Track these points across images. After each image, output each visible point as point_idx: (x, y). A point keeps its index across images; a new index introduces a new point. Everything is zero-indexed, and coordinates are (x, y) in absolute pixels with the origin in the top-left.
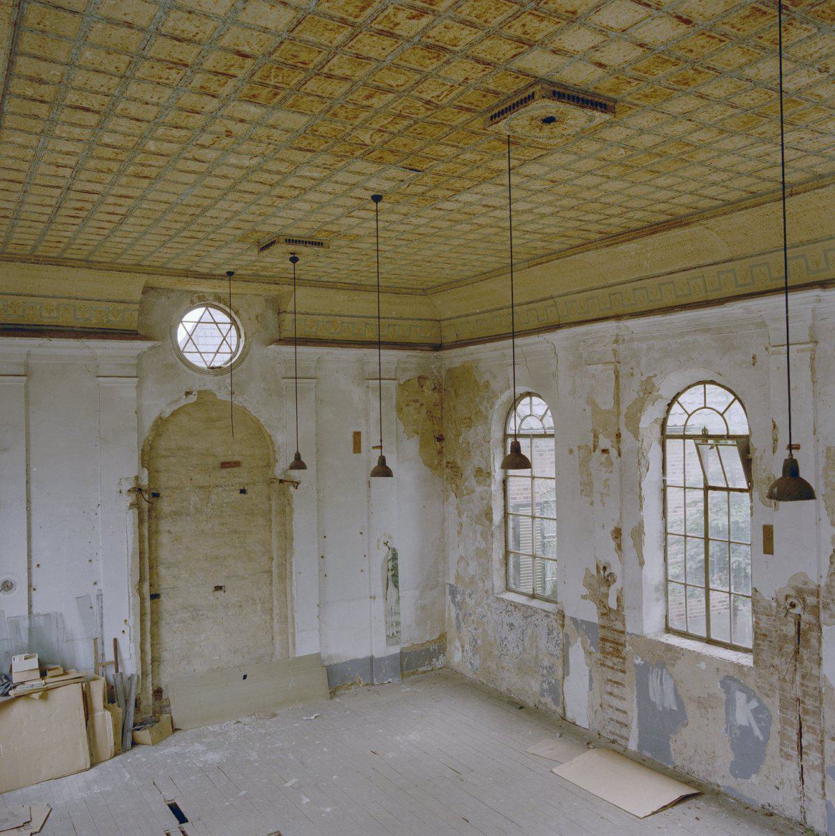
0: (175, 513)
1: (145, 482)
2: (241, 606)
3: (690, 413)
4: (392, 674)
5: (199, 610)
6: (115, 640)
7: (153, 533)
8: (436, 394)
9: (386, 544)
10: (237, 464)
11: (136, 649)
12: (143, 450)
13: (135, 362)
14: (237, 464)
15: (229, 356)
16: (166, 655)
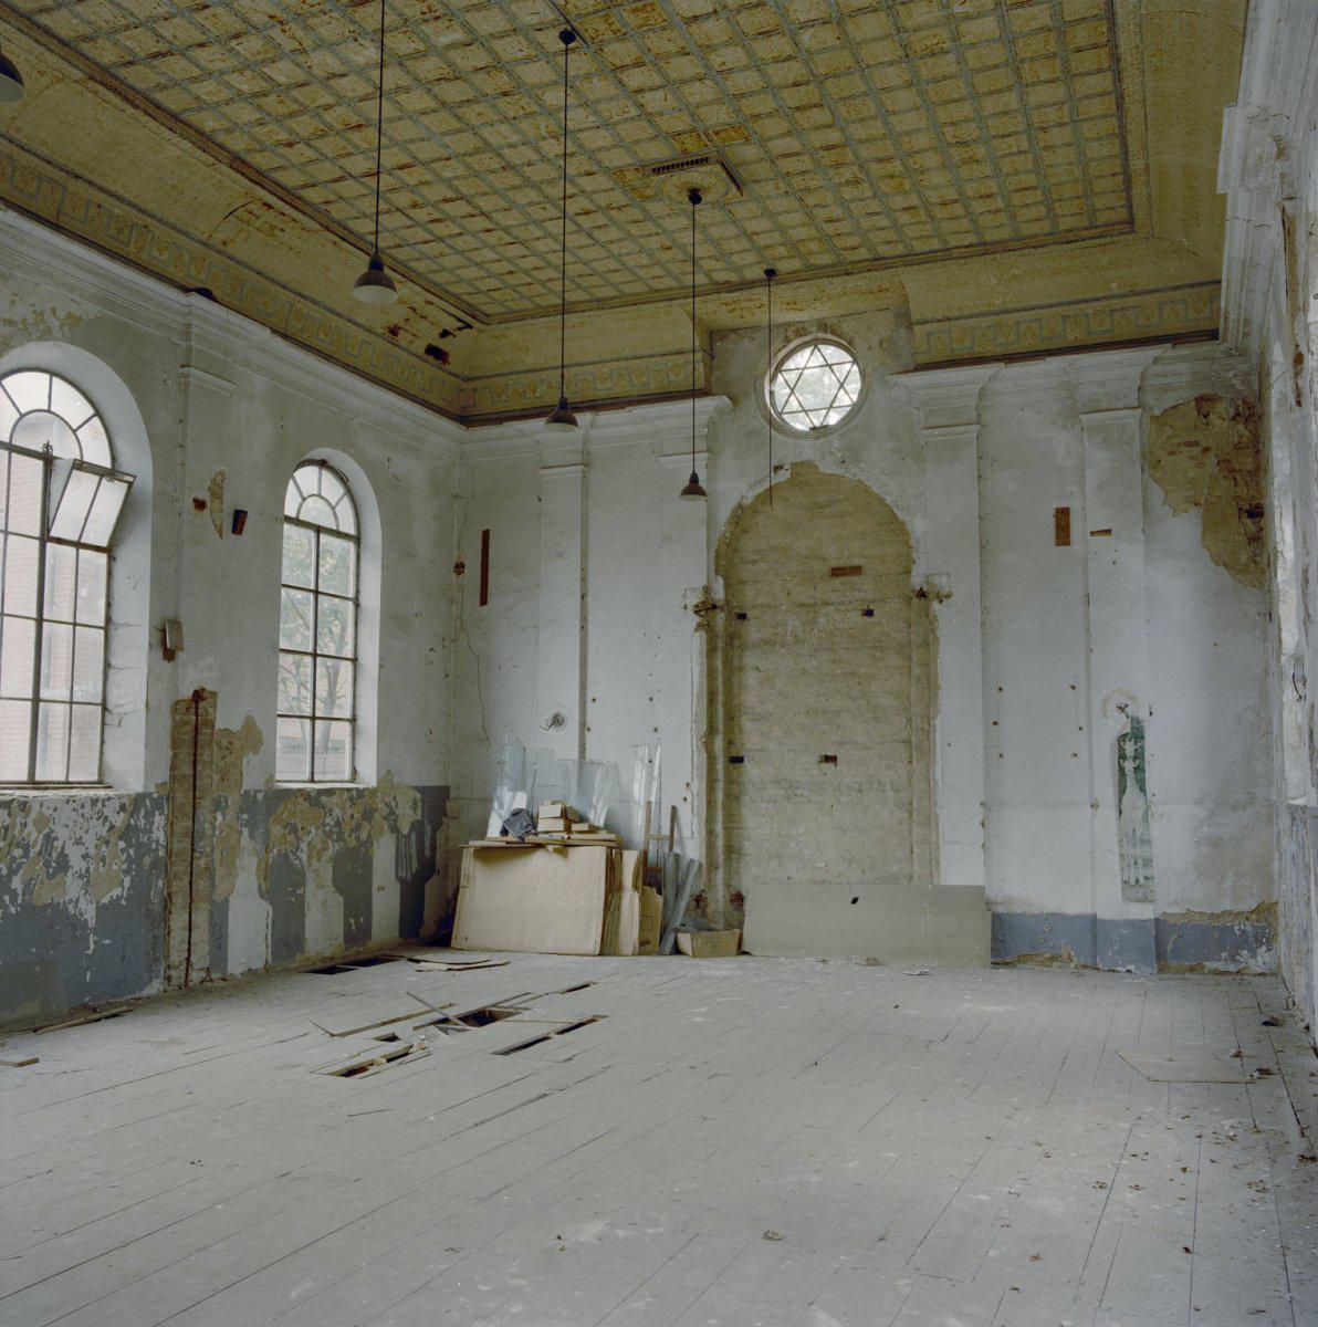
0: (766, 642)
1: (719, 594)
2: (861, 791)
4: (1136, 958)
5: (797, 788)
6: (674, 809)
7: (732, 670)
8: (1241, 427)
9: (1122, 709)
10: (856, 570)
11: (699, 825)
12: (717, 552)
14: (856, 570)
16: (749, 847)
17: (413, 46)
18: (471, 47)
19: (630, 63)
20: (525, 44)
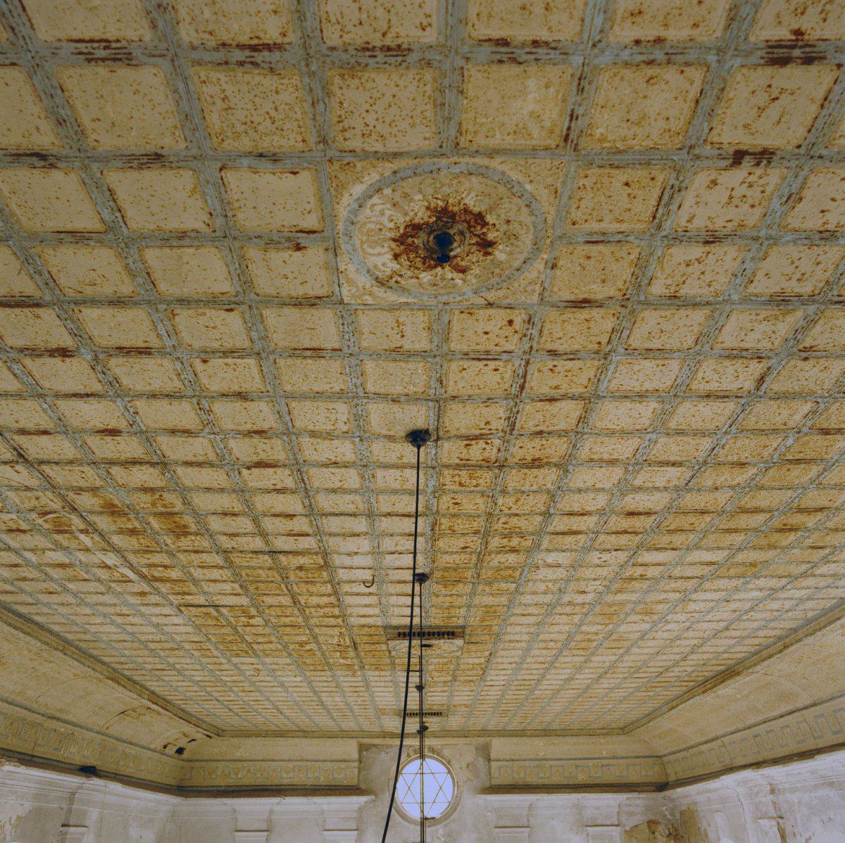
13: (355, 815)
15: (447, 804)
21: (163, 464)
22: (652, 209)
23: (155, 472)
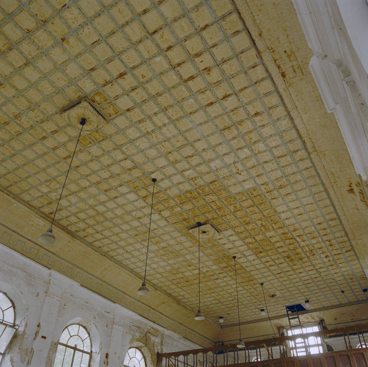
3: (71, 335)
17: (200, 168)
18: (182, 170)
19: (133, 170)
20: (166, 173)
21: (293, 270)
22: (181, 145)
23: (294, 268)
